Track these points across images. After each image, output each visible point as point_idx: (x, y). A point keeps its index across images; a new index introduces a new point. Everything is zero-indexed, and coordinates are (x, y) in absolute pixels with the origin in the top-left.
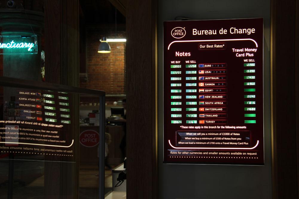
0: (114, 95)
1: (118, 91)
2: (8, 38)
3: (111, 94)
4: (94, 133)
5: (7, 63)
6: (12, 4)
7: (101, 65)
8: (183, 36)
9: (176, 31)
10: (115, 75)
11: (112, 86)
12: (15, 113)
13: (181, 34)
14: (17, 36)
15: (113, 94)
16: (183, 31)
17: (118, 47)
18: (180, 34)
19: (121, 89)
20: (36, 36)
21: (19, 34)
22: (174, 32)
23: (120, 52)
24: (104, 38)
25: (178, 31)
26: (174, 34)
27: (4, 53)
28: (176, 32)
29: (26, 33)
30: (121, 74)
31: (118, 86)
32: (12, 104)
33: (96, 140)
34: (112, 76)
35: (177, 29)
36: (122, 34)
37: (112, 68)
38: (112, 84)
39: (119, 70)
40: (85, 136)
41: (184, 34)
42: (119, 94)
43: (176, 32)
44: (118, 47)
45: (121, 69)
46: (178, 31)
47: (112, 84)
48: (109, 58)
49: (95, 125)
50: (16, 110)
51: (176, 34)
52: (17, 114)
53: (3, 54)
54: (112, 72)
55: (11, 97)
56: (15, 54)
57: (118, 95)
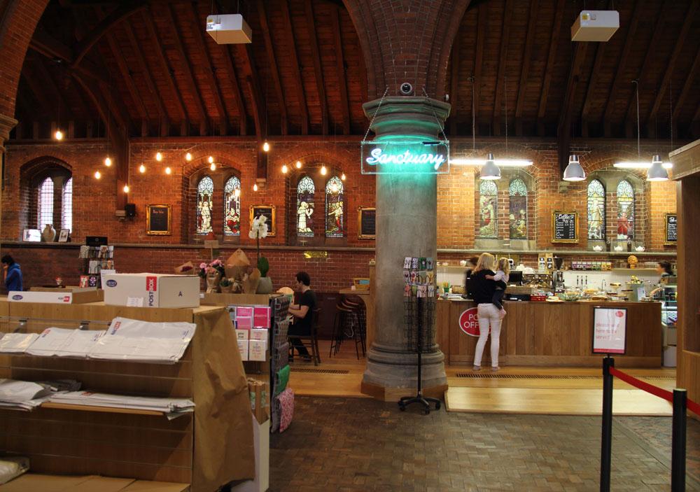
0: (459, 250)
2: (394, 145)
3: (454, 248)
5: (391, 190)
11: (456, 236)
15: (457, 248)
17: (465, 174)
19: (470, 240)
20: (448, 142)
23: (469, 182)
27: (382, 171)
30: (470, 217)
31: (464, 236)
32: (424, 263)
37: (454, 207)
38: (455, 232)
39: (467, 210)
40: (470, 318)
42: (467, 248)
44: (465, 174)
45: (470, 209)
47: (455, 232)
48: (450, 191)
53: (376, 173)
54: (456, 213)
56: (406, 174)
57: (465, 250)
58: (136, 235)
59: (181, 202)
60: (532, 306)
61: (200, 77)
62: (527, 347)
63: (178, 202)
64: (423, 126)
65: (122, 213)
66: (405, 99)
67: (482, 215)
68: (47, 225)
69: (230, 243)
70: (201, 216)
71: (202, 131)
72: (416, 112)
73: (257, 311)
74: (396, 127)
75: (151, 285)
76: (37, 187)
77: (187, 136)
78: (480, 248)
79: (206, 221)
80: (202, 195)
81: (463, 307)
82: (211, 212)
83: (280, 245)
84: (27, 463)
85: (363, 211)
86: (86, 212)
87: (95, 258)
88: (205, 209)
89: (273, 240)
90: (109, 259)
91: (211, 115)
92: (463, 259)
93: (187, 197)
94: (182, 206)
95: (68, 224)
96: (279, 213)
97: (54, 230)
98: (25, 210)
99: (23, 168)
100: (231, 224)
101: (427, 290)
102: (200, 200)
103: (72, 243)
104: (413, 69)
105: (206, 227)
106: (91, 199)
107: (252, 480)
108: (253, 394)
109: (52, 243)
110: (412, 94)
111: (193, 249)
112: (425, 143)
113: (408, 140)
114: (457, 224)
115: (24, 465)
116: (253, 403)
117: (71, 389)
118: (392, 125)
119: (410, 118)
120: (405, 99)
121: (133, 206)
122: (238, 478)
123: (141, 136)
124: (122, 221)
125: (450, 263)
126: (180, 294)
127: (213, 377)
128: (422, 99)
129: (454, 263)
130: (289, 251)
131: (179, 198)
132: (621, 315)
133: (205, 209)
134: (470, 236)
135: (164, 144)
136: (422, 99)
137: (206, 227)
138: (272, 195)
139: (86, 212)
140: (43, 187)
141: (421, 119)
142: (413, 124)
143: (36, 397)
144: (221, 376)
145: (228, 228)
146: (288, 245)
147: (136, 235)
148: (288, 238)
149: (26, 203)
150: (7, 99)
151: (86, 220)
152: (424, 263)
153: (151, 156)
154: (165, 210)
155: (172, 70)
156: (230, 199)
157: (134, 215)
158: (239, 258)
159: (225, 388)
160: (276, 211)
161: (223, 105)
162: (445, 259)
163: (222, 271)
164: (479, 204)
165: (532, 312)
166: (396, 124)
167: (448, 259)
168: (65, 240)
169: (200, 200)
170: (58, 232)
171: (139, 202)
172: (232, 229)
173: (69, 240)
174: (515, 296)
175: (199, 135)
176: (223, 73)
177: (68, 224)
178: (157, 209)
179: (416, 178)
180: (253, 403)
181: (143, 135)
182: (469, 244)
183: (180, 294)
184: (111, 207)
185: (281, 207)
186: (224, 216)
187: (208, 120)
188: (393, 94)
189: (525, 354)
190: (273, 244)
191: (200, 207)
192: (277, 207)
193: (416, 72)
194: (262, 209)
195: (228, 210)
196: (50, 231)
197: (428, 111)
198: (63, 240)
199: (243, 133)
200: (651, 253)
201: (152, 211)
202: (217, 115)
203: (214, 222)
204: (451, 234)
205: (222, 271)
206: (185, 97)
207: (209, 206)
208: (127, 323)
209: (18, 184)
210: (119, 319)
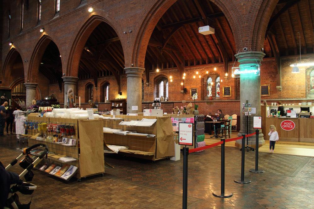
1: (302, 97)
4: (291, 122)
6: (246, 49)
7: (290, 81)
8: (292, 128)
9: (285, 123)
10: (299, 86)
12: (249, 110)
13: (290, 127)
14: (248, 66)
16: (293, 124)
18: (289, 127)
19: (304, 95)
20: (259, 65)
21: (249, 65)
22: (283, 124)
24: (295, 64)
25: (287, 124)
26: (284, 126)
28: (286, 124)
29: (253, 64)
30: (303, 86)
31: (301, 94)
32: (247, 105)
33: (292, 126)
34: (297, 87)
35: (286, 122)
36: (303, 61)
37: (297, 83)
38: (297, 92)
41: (293, 127)
42: (302, 98)
43: (286, 124)
46: (287, 124)
47: (297, 92)
48: (295, 76)
49: (291, 117)
50: (249, 108)
51: (285, 126)
52: (250, 110)
54: (297, 85)
55: (246, 101)
58: (187, 98)
59: (201, 87)
60: (310, 119)
61: (204, 45)
62: (308, 135)
63: (200, 87)
64: (252, 60)
65: (183, 91)
66: (245, 53)
67: (311, 85)
68: (161, 96)
69: (217, 100)
70: (208, 91)
71: (207, 62)
72: (249, 56)
73: (191, 119)
74: (244, 62)
75: (150, 112)
76: (159, 84)
77: (196, 65)
78: (310, 98)
79: (210, 92)
80: (209, 84)
81: (282, 120)
82: (212, 89)
83: (233, 100)
84: (128, 147)
85: (262, 86)
86: (172, 91)
87: (156, 106)
88: (210, 88)
89: (231, 98)
90: (160, 106)
91: (209, 56)
92: (299, 103)
93: (204, 85)
94: (201, 88)
95: (167, 96)
96: (232, 89)
97: (164, 98)
98: (156, 92)
99: (155, 79)
100: (218, 93)
101: (248, 113)
102: (208, 85)
103: (169, 101)
104: (247, 42)
105: (210, 95)
106: (174, 87)
107: (174, 156)
108: (175, 137)
109: (163, 102)
110: (247, 51)
111: (205, 102)
112: (251, 66)
113: (248, 65)
114: (298, 89)
115: (127, 148)
116: (175, 138)
117: (135, 133)
118: (242, 61)
119: (247, 59)
120: (245, 53)
121: (186, 89)
122: (171, 156)
123: (188, 66)
124: (183, 94)
125: (295, 104)
126: (157, 113)
127: (164, 132)
128: (250, 52)
129: (297, 104)
130: (236, 102)
131: (200, 85)
132: (260, 118)
133: (210, 88)
134: (303, 94)
135: (195, 68)
136: (250, 52)
137: (210, 95)
138: (230, 82)
139: (172, 91)
140: (161, 84)
141: (250, 58)
142: (248, 60)
143: (127, 133)
144: (166, 131)
145: (217, 95)
146: (237, 100)
147: (187, 98)
148: (237, 97)
149: (156, 89)
150: (142, 63)
151: (172, 94)
152: (247, 105)
153: (212, 68)
154: (196, 89)
155: (194, 44)
156: (218, 85)
157: (186, 92)
158: (190, 105)
159: (167, 134)
160: (232, 88)
161: (213, 53)
162: (289, 103)
163: (185, 109)
164: (310, 80)
165: (310, 122)
166: (244, 61)
167: (294, 103)
168: (166, 101)
169: (208, 85)
170: (165, 98)
171: (188, 87)
172: (219, 95)
173: (168, 100)
174: (303, 116)
175: (206, 64)
176: (210, 43)
177: (167, 96)
178: (193, 89)
179: (250, 78)
180: (175, 138)
181: (188, 65)
182: (303, 97)
183: (157, 113)
184: (180, 90)
185: (234, 86)
186: (216, 90)
187: (209, 58)
188: (242, 51)
189: (308, 138)
190: (231, 99)
191: (208, 88)
192: (232, 86)
193: (248, 43)
194: (227, 87)
195: (217, 88)
196: (162, 98)
197: (253, 55)
198: (166, 101)
199: (213, 62)
200: (285, 99)
201: (192, 90)
202: (211, 56)
203: (213, 92)
204: (295, 93)
205: (185, 109)
206: (200, 52)
207: (211, 87)
208: (145, 119)
209: (153, 84)
210: (144, 119)
